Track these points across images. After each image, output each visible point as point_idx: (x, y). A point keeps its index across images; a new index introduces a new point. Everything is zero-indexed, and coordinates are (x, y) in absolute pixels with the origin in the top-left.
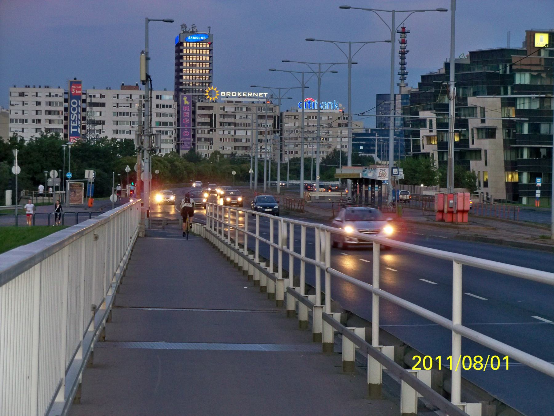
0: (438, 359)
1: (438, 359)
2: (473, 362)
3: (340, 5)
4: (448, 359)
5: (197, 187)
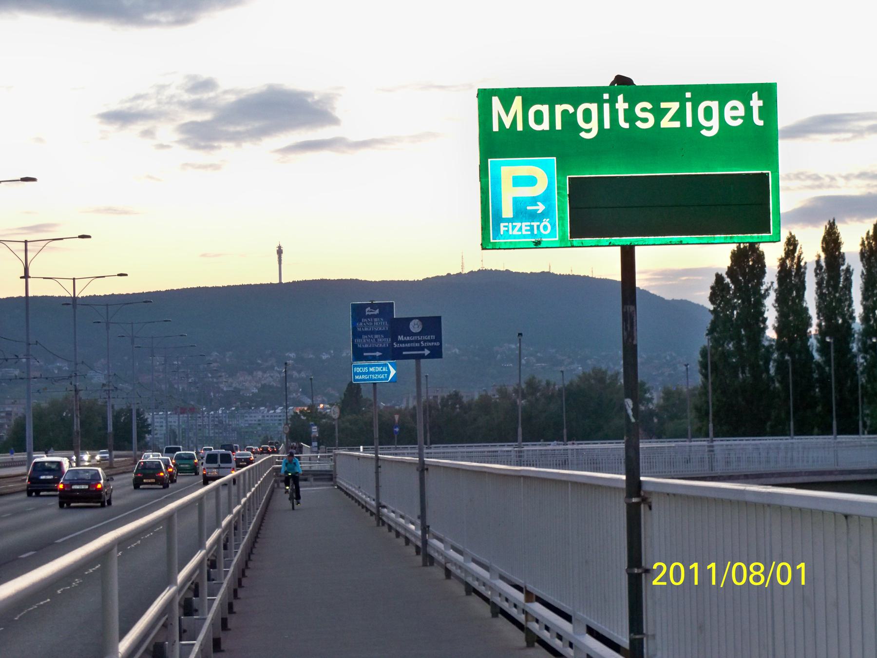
0: (711, 569)
1: (711, 569)
2: (749, 573)
3: (283, 249)
4: (709, 567)
5: (323, 408)
